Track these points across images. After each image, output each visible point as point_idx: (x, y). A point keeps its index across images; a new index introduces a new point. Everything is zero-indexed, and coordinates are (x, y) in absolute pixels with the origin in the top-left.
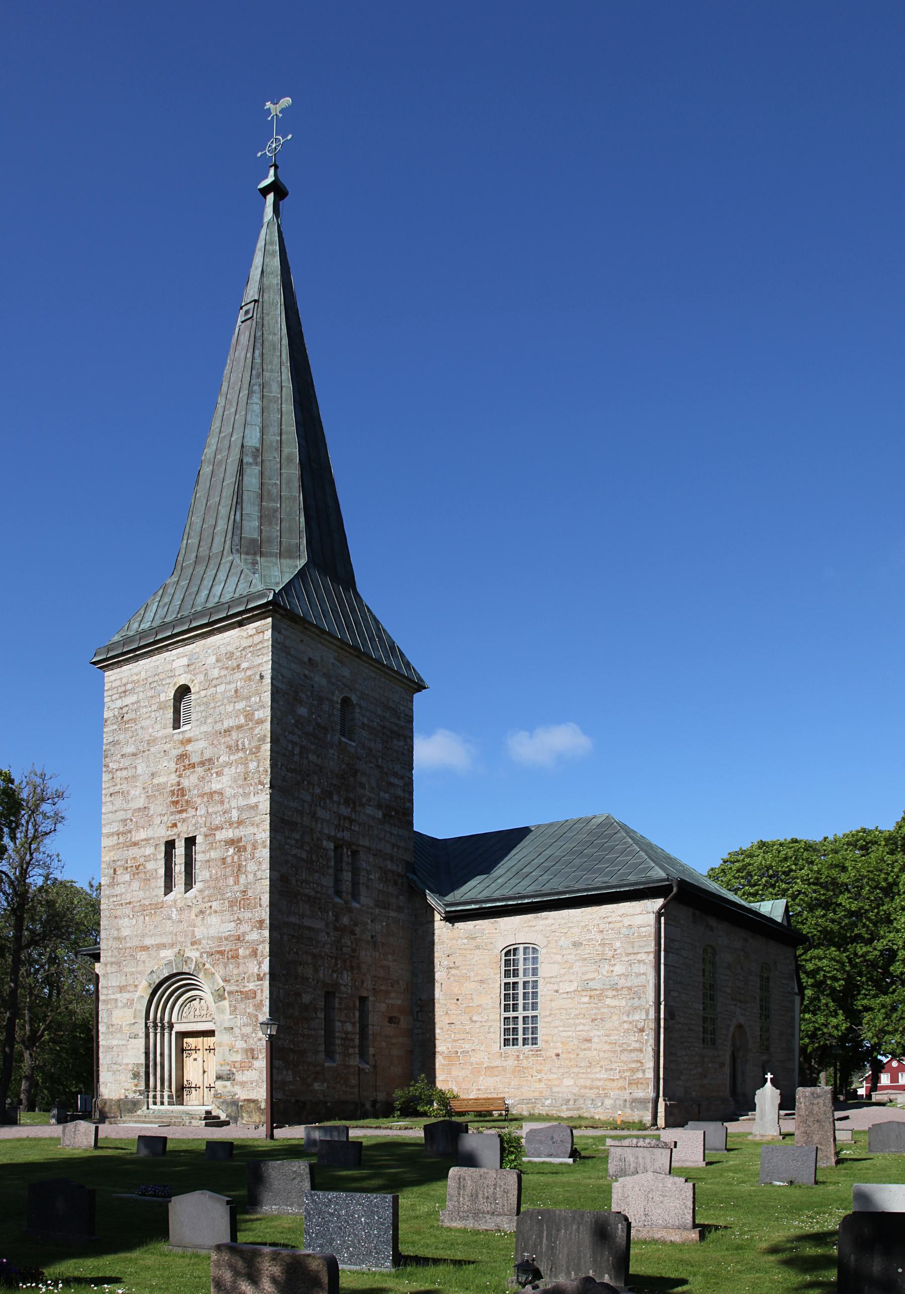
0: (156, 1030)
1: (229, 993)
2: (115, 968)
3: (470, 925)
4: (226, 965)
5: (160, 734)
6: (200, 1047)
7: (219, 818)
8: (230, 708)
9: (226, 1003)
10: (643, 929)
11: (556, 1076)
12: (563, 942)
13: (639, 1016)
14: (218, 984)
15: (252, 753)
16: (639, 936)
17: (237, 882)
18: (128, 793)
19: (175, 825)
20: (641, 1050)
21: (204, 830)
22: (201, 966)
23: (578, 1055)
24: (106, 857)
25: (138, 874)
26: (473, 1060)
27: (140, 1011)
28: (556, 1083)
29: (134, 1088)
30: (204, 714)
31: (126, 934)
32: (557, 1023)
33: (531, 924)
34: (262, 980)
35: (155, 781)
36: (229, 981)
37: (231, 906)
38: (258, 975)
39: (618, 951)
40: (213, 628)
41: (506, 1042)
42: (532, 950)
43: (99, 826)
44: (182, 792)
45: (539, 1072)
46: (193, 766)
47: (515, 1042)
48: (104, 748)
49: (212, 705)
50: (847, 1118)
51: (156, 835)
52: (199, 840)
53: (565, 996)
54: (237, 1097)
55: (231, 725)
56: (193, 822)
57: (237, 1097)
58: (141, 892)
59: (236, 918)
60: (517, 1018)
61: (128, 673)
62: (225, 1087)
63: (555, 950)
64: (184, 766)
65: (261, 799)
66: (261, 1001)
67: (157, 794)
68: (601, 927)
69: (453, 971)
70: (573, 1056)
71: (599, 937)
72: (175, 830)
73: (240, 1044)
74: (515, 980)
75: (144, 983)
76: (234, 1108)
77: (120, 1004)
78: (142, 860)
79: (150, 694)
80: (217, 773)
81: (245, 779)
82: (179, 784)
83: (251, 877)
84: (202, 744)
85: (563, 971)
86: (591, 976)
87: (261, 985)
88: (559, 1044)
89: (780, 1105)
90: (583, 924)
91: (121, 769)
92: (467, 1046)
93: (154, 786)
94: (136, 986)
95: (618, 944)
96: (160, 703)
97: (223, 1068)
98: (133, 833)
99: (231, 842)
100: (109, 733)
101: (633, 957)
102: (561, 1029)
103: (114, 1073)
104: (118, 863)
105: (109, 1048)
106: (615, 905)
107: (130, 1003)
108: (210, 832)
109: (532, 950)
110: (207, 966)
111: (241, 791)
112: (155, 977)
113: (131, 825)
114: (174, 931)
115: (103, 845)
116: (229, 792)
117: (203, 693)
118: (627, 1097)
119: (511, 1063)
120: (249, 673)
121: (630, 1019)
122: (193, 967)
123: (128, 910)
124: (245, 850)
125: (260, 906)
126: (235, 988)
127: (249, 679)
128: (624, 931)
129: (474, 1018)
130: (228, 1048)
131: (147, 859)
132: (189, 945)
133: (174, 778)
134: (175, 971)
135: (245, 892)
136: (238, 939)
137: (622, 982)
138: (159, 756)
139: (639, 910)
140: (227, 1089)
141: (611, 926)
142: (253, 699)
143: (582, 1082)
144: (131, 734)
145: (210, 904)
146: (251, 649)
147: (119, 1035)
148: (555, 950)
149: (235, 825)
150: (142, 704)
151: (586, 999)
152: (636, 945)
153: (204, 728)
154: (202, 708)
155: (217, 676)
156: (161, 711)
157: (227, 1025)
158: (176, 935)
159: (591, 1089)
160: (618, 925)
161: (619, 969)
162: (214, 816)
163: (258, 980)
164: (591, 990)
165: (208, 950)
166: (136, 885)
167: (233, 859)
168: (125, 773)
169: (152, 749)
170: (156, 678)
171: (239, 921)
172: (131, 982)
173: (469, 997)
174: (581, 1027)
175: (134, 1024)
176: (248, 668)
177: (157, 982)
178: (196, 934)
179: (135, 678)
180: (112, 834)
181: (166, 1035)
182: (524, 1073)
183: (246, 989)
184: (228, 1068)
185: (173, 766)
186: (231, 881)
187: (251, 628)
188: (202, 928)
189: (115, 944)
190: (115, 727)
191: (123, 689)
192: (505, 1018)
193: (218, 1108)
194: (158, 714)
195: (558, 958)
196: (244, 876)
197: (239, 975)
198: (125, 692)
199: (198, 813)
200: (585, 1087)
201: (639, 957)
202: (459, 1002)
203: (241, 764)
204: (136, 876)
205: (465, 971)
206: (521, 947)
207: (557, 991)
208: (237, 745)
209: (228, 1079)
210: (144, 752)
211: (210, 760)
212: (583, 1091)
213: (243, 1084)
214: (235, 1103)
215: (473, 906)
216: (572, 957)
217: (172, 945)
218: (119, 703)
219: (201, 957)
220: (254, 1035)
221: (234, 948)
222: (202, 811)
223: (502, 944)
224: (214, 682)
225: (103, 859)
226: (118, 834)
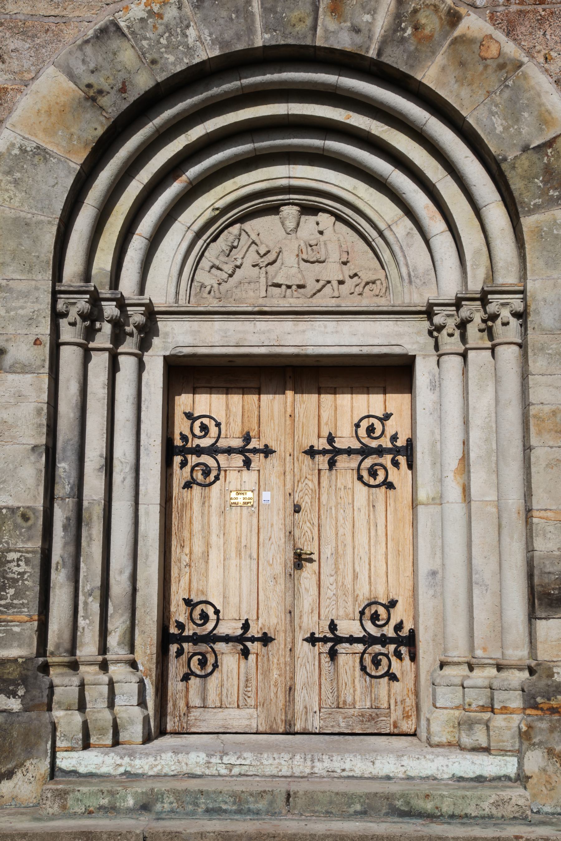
0: (90, 333)
6: (270, 436)
22: (430, 23)
75: (52, 85)
89: (271, 642)
112: (127, 56)
122: (381, 23)
134: (260, 40)
177: (143, 82)
181: (127, 364)
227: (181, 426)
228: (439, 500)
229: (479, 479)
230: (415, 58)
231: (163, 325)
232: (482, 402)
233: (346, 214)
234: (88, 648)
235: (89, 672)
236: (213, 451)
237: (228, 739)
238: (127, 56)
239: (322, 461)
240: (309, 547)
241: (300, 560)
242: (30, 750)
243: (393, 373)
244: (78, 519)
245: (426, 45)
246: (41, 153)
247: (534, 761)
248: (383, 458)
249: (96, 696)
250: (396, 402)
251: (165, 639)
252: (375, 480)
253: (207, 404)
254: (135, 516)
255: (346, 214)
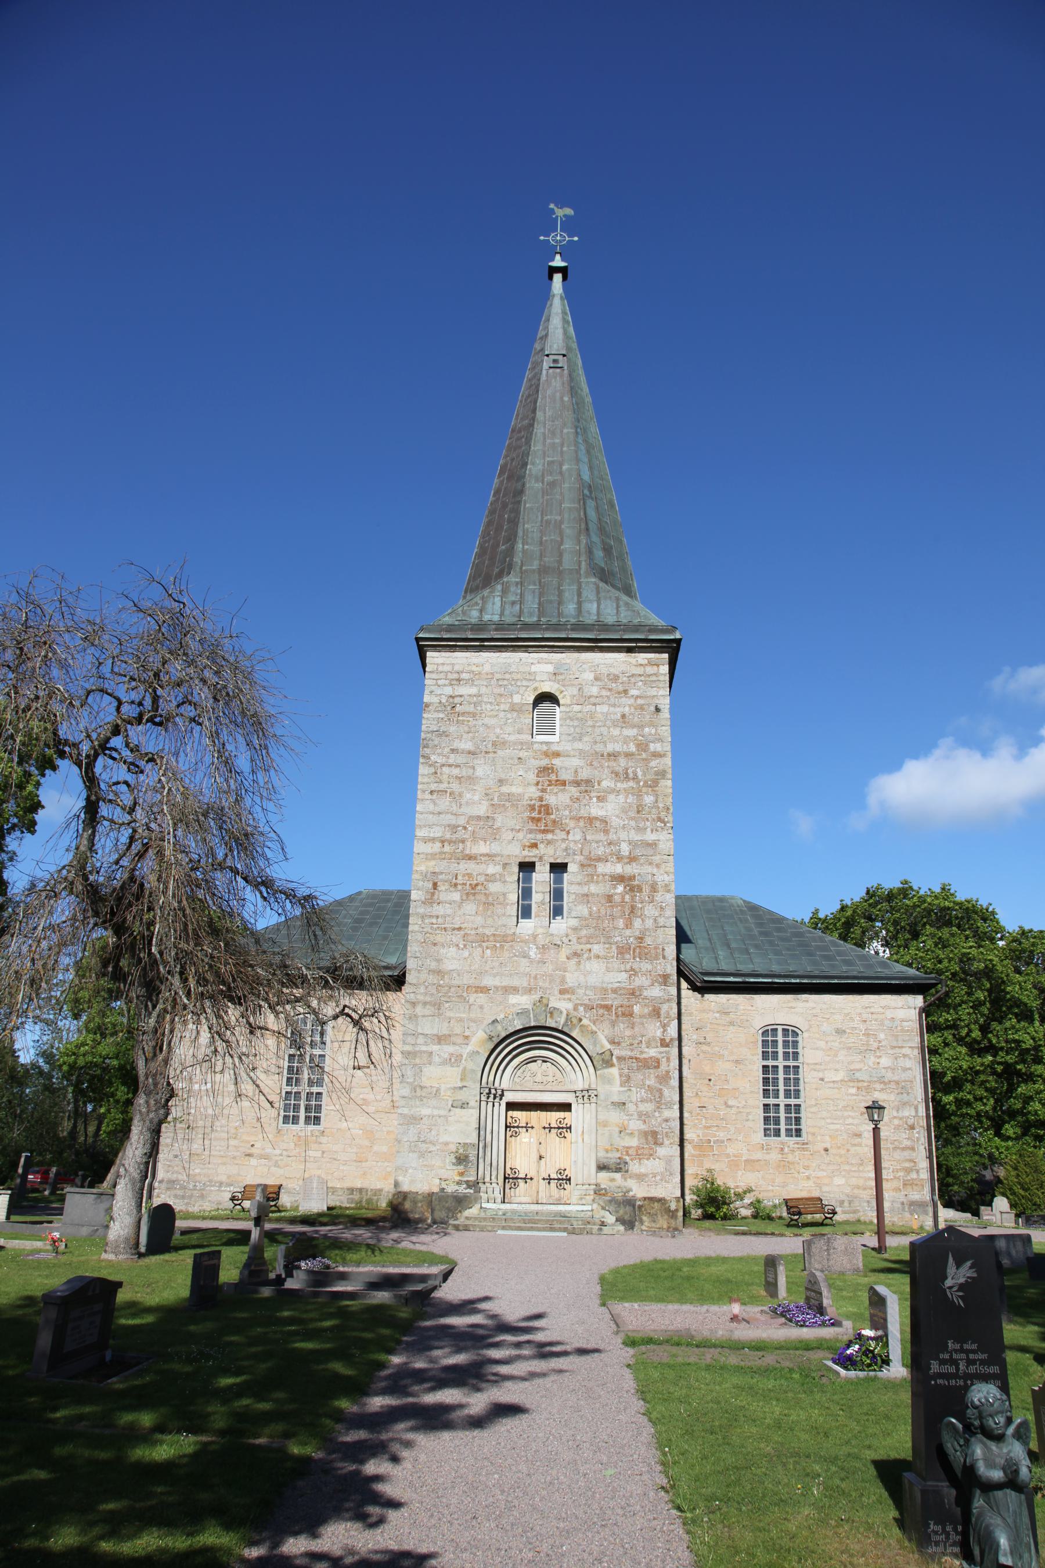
1: (619, 1058)
2: (429, 1010)
3: (722, 998)
4: (613, 1024)
5: (512, 738)
7: (602, 849)
8: (616, 732)
9: (614, 1071)
10: (905, 1024)
11: (825, 1174)
12: (825, 1027)
13: (908, 1112)
14: (602, 1047)
15: (646, 785)
16: (902, 1030)
17: (629, 925)
18: (460, 795)
19: (534, 846)
20: (913, 1149)
21: (578, 858)
22: (575, 1021)
23: (848, 1150)
24: (421, 866)
25: (474, 895)
26: (729, 1150)
27: (473, 1071)
28: (826, 1181)
29: (457, 1178)
30: (578, 730)
31: (451, 967)
32: (824, 1114)
33: (790, 1005)
34: (667, 1046)
35: (505, 789)
36: (619, 1044)
37: (622, 953)
38: (662, 1040)
39: (883, 1043)
40: (596, 645)
41: (286, 1120)
42: (791, 1033)
43: (411, 826)
44: (547, 809)
45: (806, 1168)
46: (564, 783)
47: (295, 1120)
48: (423, 735)
49: (590, 723)
50: (51, 1222)
51: (506, 852)
52: (571, 868)
53: (831, 1085)
54: (631, 1194)
55: (617, 749)
56: (564, 846)
57: (631, 1194)
58: (479, 918)
59: (628, 967)
60: (778, 1105)
61: (465, 661)
62: (613, 1180)
63: (817, 1036)
64: (550, 781)
65: (662, 838)
66: (668, 1072)
67: (508, 804)
68: (865, 1016)
69: (704, 1048)
70: (843, 1152)
71: (862, 1027)
72: (535, 852)
73: (636, 1125)
74: (775, 1063)
75: (481, 1035)
76: (628, 1209)
77: (436, 1059)
78: (481, 879)
79: (497, 691)
80: (598, 797)
81: (638, 812)
82: (541, 799)
83: (649, 923)
84: (576, 762)
85: (827, 1059)
86: (858, 1066)
87: (667, 1053)
88: (827, 1138)
90: (846, 1011)
91: (450, 766)
92: (722, 1135)
93: (502, 794)
94: (467, 1037)
95: (882, 1036)
96: (513, 705)
97: (609, 1155)
98: (468, 844)
99: (620, 879)
100: (430, 721)
101: (897, 1050)
102: (829, 1121)
103: (422, 1155)
104: (440, 877)
105: (415, 1119)
106: (876, 996)
107: (454, 1060)
108: (589, 862)
109: (791, 1033)
110: (585, 1022)
111: (633, 823)
112: (499, 1028)
113: (461, 834)
114: (533, 973)
115: (416, 850)
116: (615, 822)
117: (577, 708)
118: (903, 1199)
119: (774, 1156)
120: (640, 701)
121: (900, 1114)
122: (562, 1020)
123: (457, 937)
124: (640, 890)
125: (664, 957)
126: (627, 1053)
127: (641, 708)
128: (887, 1022)
129: (730, 1103)
130: (617, 1130)
131: (490, 878)
132: (556, 992)
133: (533, 792)
135: (641, 938)
136: (633, 994)
137: (889, 1075)
138: (511, 761)
139: (900, 1005)
140: (616, 1184)
141: (875, 1016)
142: (647, 730)
143: (854, 1181)
144: (466, 729)
145: (589, 946)
146: (642, 678)
147: (433, 1102)
148: (817, 1036)
149: (626, 861)
150: (485, 700)
151: (853, 1091)
152: (900, 1038)
153: (579, 745)
154: (576, 723)
155: (595, 694)
156: (515, 714)
157: (616, 1099)
158: (535, 978)
159: (865, 1189)
160: (881, 1017)
161: (885, 1061)
162: (594, 845)
163: (662, 1045)
164: (859, 1081)
165: (587, 1002)
166: (470, 907)
167: (623, 898)
168: (456, 771)
169: (500, 753)
170: (507, 676)
171: (633, 972)
172: (458, 1031)
173: (723, 1077)
174: (850, 1121)
175: (461, 1088)
176: (637, 697)
177: (503, 1035)
178: (568, 980)
179: (474, 668)
180: (433, 840)
182: (790, 1169)
183: (644, 1056)
184: (618, 1155)
185: (532, 777)
186: (621, 923)
187: (643, 657)
188: (576, 974)
189: (432, 979)
190: (441, 715)
191: (456, 676)
192: (287, 1093)
193: (603, 1208)
194: (509, 716)
195: (822, 1044)
196: (639, 920)
197: (634, 1037)
198: (459, 680)
199: (571, 837)
200: (858, 1187)
201: (904, 1051)
202: (711, 1083)
203: (633, 794)
204: (471, 897)
205: (717, 1048)
206: (780, 1028)
207: (822, 1079)
208: (627, 773)
209: (618, 1170)
210: (486, 752)
211: (588, 782)
212: (856, 1191)
213: (640, 1177)
214: (630, 1202)
215: (732, 979)
216: (837, 1044)
217: (529, 991)
218: (448, 691)
219: (575, 1009)
220: (657, 1114)
221: (625, 1003)
222: (576, 835)
223: (759, 1022)
224: (592, 700)
225: (415, 868)
226: (443, 842)
227: (509, 1120)
228: (576, 1142)
229: (586, 1137)
230: (570, 1030)
231: (505, 1093)
232: (588, 1117)
233: (554, 1063)
234: (487, 1179)
235: (488, 1185)
236: (518, 1127)
237: (522, 1198)
238: (499, 1028)
239: (547, 1130)
240: (543, 1154)
241: (541, 1157)
242: (476, 1202)
243: (566, 1107)
244: (485, 1146)
245: (574, 1026)
246: (478, 1052)
247: (595, 1206)
248: (563, 1129)
249: (490, 1191)
250: (567, 1114)
251: (505, 1178)
252: (561, 1135)
253: (516, 1114)
254: (498, 1145)
255: (554, 1063)
